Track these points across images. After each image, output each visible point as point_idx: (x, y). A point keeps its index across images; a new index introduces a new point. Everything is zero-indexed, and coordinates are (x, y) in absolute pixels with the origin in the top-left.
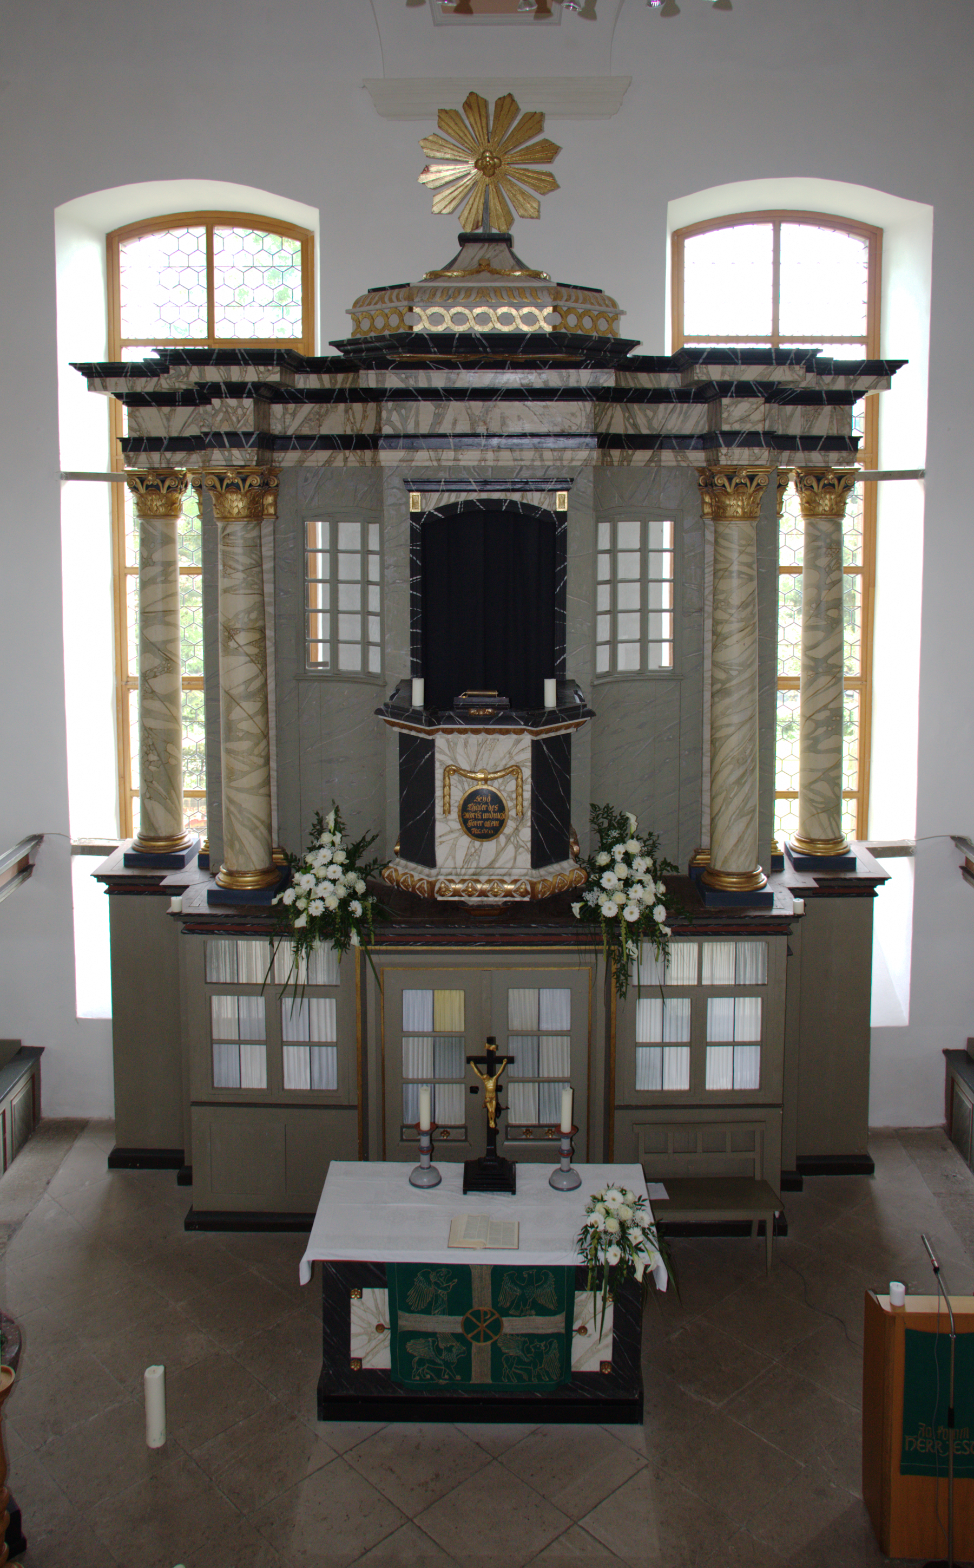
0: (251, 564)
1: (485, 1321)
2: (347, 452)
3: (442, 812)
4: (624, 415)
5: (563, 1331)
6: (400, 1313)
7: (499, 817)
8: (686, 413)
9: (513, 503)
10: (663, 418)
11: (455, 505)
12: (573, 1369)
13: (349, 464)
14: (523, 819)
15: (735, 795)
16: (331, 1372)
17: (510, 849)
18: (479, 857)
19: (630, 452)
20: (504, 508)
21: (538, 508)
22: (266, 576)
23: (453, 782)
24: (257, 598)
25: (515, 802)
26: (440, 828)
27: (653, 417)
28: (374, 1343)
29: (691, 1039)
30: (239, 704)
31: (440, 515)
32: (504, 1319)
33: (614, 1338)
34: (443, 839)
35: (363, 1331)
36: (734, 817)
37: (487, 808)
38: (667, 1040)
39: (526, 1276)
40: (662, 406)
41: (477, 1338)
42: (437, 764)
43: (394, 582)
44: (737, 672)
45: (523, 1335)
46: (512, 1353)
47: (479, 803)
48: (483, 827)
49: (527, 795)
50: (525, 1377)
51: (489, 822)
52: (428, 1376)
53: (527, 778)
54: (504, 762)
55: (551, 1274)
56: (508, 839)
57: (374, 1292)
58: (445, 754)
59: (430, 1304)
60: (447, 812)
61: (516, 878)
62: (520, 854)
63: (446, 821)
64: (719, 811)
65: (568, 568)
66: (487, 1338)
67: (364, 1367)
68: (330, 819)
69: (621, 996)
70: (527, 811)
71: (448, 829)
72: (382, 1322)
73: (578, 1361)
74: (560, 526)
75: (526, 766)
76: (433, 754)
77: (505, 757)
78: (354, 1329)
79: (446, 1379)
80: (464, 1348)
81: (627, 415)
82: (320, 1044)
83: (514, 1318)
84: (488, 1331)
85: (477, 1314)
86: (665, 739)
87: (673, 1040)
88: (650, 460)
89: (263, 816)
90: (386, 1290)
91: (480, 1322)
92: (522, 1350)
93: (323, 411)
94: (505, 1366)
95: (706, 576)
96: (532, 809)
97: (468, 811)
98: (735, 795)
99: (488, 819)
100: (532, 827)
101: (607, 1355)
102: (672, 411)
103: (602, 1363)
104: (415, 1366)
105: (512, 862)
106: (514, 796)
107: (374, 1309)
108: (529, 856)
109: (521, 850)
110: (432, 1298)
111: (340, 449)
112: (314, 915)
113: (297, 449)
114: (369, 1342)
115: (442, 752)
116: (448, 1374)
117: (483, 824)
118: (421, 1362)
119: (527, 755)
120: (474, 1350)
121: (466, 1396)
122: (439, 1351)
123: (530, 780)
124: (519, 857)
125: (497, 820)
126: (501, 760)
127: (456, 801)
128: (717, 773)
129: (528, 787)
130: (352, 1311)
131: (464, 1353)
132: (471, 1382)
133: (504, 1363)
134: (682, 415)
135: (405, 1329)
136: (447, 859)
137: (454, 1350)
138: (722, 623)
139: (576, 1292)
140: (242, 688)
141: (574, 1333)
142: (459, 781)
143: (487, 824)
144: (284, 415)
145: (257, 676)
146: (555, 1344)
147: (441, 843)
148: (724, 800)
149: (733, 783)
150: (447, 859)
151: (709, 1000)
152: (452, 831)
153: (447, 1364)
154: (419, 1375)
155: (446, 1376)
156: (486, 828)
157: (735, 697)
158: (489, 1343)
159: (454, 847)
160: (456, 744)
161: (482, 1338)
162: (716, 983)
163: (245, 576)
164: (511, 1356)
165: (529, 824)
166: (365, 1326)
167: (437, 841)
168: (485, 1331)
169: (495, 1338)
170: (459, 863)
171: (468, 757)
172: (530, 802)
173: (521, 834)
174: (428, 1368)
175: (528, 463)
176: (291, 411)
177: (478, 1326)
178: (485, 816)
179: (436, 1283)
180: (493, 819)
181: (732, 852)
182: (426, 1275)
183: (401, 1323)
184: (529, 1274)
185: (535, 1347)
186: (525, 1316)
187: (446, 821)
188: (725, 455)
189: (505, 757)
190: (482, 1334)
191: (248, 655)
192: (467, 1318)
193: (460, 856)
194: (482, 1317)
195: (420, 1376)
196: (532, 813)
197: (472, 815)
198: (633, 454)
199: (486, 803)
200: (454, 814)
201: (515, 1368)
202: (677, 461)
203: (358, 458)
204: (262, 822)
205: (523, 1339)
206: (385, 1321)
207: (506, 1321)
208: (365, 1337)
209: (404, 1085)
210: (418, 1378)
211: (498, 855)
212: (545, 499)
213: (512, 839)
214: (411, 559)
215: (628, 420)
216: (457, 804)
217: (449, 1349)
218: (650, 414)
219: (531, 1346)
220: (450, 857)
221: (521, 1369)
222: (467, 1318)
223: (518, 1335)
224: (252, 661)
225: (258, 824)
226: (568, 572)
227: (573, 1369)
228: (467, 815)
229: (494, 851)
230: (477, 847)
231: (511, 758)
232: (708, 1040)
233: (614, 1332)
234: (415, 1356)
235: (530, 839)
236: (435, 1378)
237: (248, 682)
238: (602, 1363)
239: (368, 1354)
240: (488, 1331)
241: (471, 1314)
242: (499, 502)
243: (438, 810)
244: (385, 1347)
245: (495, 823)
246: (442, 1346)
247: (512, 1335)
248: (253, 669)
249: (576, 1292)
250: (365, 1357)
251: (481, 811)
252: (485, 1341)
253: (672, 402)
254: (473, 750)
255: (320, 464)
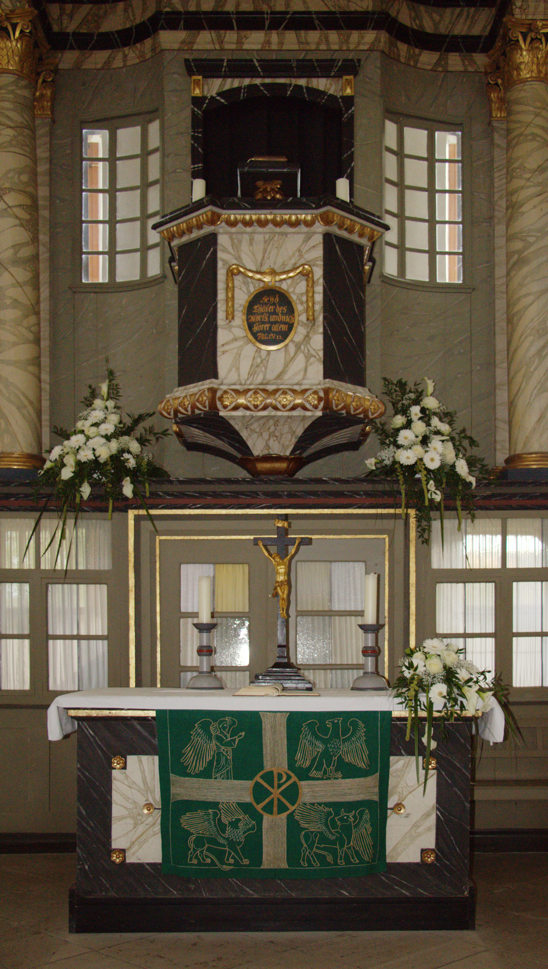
0: (22, 123)
1: (279, 786)
2: (126, 49)
3: (225, 318)
4: (410, 15)
5: (376, 798)
6: (172, 777)
7: (288, 320)
8: (473, 16)
9: (298, 88)
10: (450, 22)
11: (239, 89)
12: (388, 860)
13: (129, 63)
14: (314, 324)
15: (535, 370)
16: (87, 867)
17: (300, 360)
18: (266, 368)
19: (417, 51)
20: (289, 93)
21: (323, 93)
22: (40, 179)
23: (236, 283)
24: (28, 162)
25: (305, 305)
26: (222, 336)
27: (439, 22)
28: (141, 828)
29: (496, 629)
30: (7, 270)
31: (223, 101)
32: (303, 783)
33: (438, 817)
34: (226, 348)
35: (127, 813)
36: (535, 392)
37: (275, 309)
38: (469, 631)
39: (330, 726)
40: (448, 11)
41: (268, 809)
42: (220, 264)
43: (175, 171)
44: (535, 238)
45: (327, 804)
46: (313, 827)
47: (266, 304)
48: (270, 331)
49: (319, 297)
50: (330, 859)
51: (277, 325)
52: (209, 861)
53: (319, 279)
54: (293, 261)
55: (360, 723)
56: (298, 347)
57: (140, 761)
58: (229, 253)
59: (211, 763)
60: (230, 316)
61: (307, 387)
62: (311, 364)
63: (229, 328)
64: (519, 388)
65: (355, 155)
66: (282, 808)
67: (128, 861)
68: (104, 388)
69: (423, 542)
70: (319, 315)
71: (231, 337)
72: (151, 801)
73: (394, 849)
74: (347, 111)
75: (317, 266)
76: (215, 253)
77: (294, 255)
78: (116, 811)
79: (230, 865)
80: (254, 822)
81: (413, 14)
82: (89, 638)
83: (315, 782)
84: (283, 800)
85: (269, 777)
86: (456, 353)
87: (477, 631)
88: (437, 64)
89: (32, 395)
90: (156, 758)
91: (273, 787)
92: (326, 825)
93: (101, 12)
94: (305, 845)
95: (496, 180)
96: (324, 312)
97: (254, 314)
98: (535, 370)
99: (276, 323)
100: (325, 333)
101: (430, 841)
102: (459, 15)
103: (424, 852)
104: (192, 846)
105: (302, 373)
106: (304, 299)
107: (139, 782)
108: (321, 367)
109: (312, 359)
110: (214, 756)
111: (119, 47)
112: (83, 461)
113: (75, 49)
114: (134, 827)
115: (225, 250)
116: (233, 857)
117: (270, 328)
118: (199, 842)
119: (319, 252)
120: (265, 824)
121: (256, 896)
122: (222, 827)
123: (321, 281)
124: (310, 369)
125: (285, 323)
126: (290, 258)
127: (241, 305)
128: (516, 350)
129: (319, 289)
130: (113, 787)
131: (253, 828)
132: (262, 867)
133: (303, 842)
134: (469, 20)
135: (179, 798)
136: (230, 370)
137: (241, 825)
138: (516, 192)
139: (392, 758)
140: (10, 252)
141: (389, 811)
142: (244, 283)
143: (275, 328)
144: (61, 15)
145: (27, 244)
146: (367, 816)
147: (224, 352)
148: (524, 376)
149: (533, 356)
150: (230, 370)
151: (515, 584)
152: (235, 339)
153: (232, 844)
154: (197, 857)
155: (232, 861)
156: (274, 332)
157: (534, 264)
158: (284, 815)
159: (238, 357)
160: (240, 241)
161: (275, 809)
162: (521, 566)
163: (16, 134)
164: (313, 832)
165: (321, 330)
166: (130, 806)
167: (220, 350)
168: (279, 800)
169: (292, 808)
170: (244, 375)
171: (254, 255)
172: (322, 305)
173: (312, 342)
174: (209, 849)
175: (313, 47)
176: (68, 12)
177: (272, 793)
178: (273, 318)
179: (218, 738)
180: (282, 323)
181: (534, 429)
182: (205, 727)
183: (173, 790)
184: (333, 722)
185: (341, 820)
186: (328, 779)
187: (229, 328)
188: (520, 8)
189: (294, 255)
190: (276, 803)
191: (17, 217)
192: (257, 784)
193: (245, 366)
194: (276, 779)
195: (199, 859)
196: (325, 318)
197: (258, 318)
198: (420, 55)
199: (274, 304)
200: (240, 319)
201: (317, 847)
202: (464, 65)
203: (138, 52)
204: (31, 403)
205: (327, 809)
206: (154, 799)
207: (304, 785)
208: (130, 821)
209: (182, 674)
210: (195, 862)
211: (286, 366)
212: (331, 85)
213: (302, 347)
214: (193, 145)
215: (415, 21)
216: (241, 309)
217: (235, 824)
218: (436, 17)
219: (336, 818)
220: (234, 369)
221: (324, 849)
222: (257, 784)
223: (320, 804)
224: (22, 225)
225: (26, 403)
226: (355, 159)
227: (388, 860)
228: (253, 319)
229: (283, 361)
230: (263, 357)
231: (301, 256)
232: (514, 630)
233: (437, 809)
234: (192, 834)
235: (322, 347)
236: (217, 862)
237: (17, 247)
238: (424, 852)
239: (133, 843)
240: (283, 800)
241: (262, 777)
242: (284, 86)
243: (221, 315)
244: (155, 834)
245: (284, 328)
246: (225, 820)
247: (313, 804)
248: (23, 235)
249: (392, 758)
250: (130, 848)
251: (268, 313)
252: (279, 812)
253: (459, 6)
254: (259, 248)
255: (99, 66)
